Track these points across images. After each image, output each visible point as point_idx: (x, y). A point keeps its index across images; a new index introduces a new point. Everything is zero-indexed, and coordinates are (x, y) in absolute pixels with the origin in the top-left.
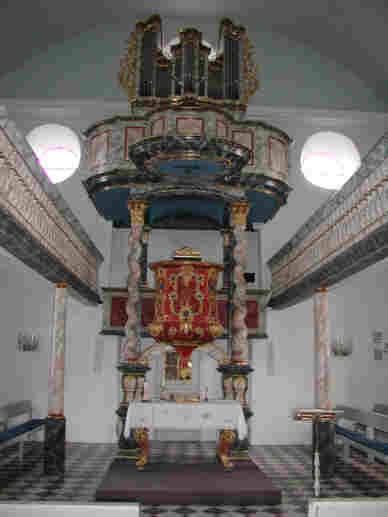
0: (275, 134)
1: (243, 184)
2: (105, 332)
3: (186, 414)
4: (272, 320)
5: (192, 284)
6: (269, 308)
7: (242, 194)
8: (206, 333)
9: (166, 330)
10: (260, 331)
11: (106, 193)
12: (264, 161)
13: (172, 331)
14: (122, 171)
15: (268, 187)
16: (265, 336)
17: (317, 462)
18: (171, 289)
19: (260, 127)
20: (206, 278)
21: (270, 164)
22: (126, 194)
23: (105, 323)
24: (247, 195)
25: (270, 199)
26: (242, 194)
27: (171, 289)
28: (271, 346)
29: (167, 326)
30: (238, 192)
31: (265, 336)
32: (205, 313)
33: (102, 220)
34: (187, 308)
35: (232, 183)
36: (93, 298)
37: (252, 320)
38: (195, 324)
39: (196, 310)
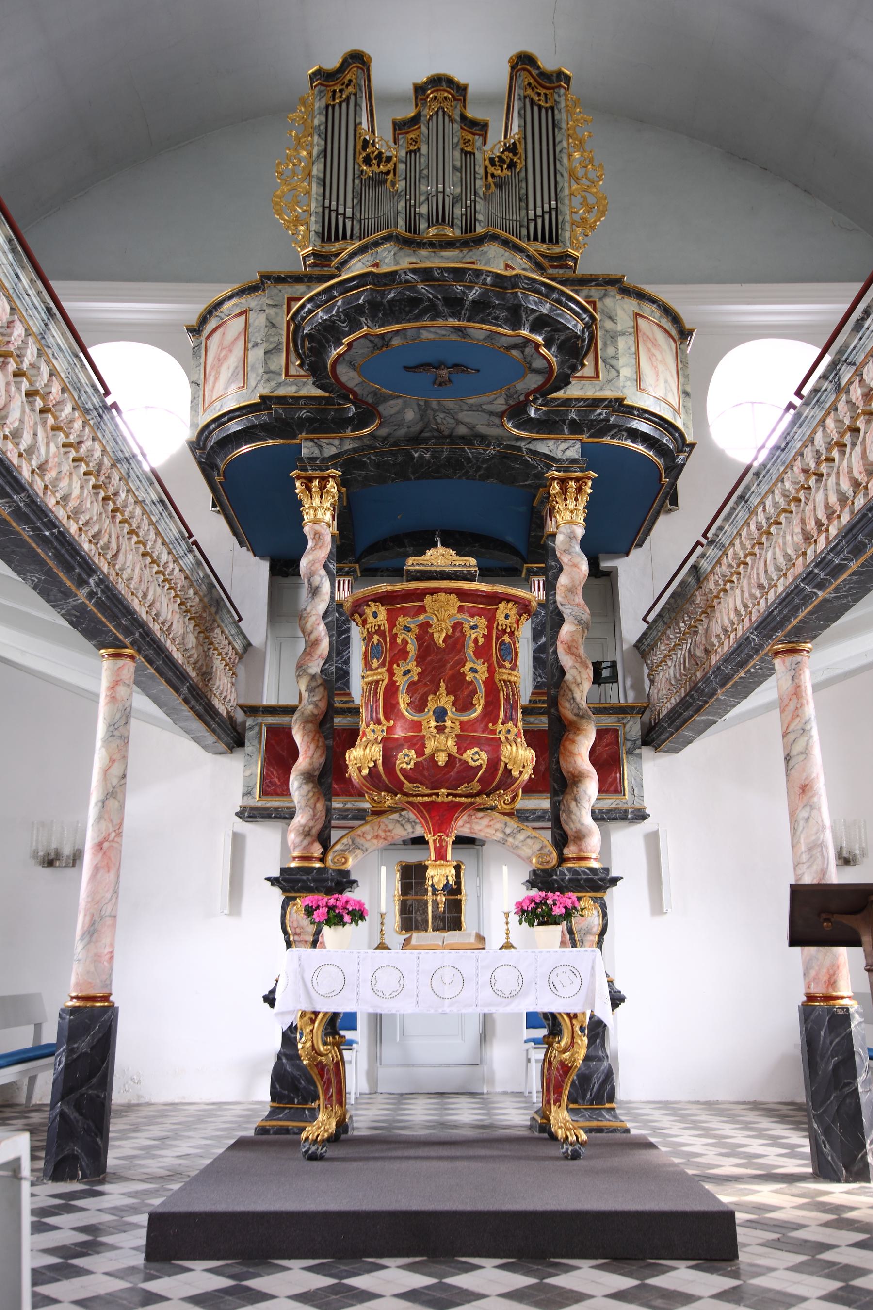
0: (648, 309)
1: (576, 428)
2: (249, 814)
3: (450, 1006)
4: (653, 776)
5: (456, 640)
6: (646, 751)
7: (574, 452)
8: (494, 762)
9: (388, 758)
10: (627, 801)
11: (245, 470)
12: (626, 372)
13: (406, 759)
14: (281, 400)
15: (635, 435)
16: (641, 816)
17: (837, 1040)
18: (403, 654)
19: (612, 291)
20: (489, 628)
21: (638, 380)
22: (295, 458)
23: (247, 793)
24: (583, 454)
25: (640, 477)
26: (574, 452)
27: (403, 654)
28: (653, 841)
29: (390, 748)
30: (566, 449)
31: (641, 816)
32: (490, 714)
33: (245, 554)
34: (445, 700)
35: (549, 426)
36: (233, 738)
37: (608, 763)
38: (464, 742)
39: (464, 705)
